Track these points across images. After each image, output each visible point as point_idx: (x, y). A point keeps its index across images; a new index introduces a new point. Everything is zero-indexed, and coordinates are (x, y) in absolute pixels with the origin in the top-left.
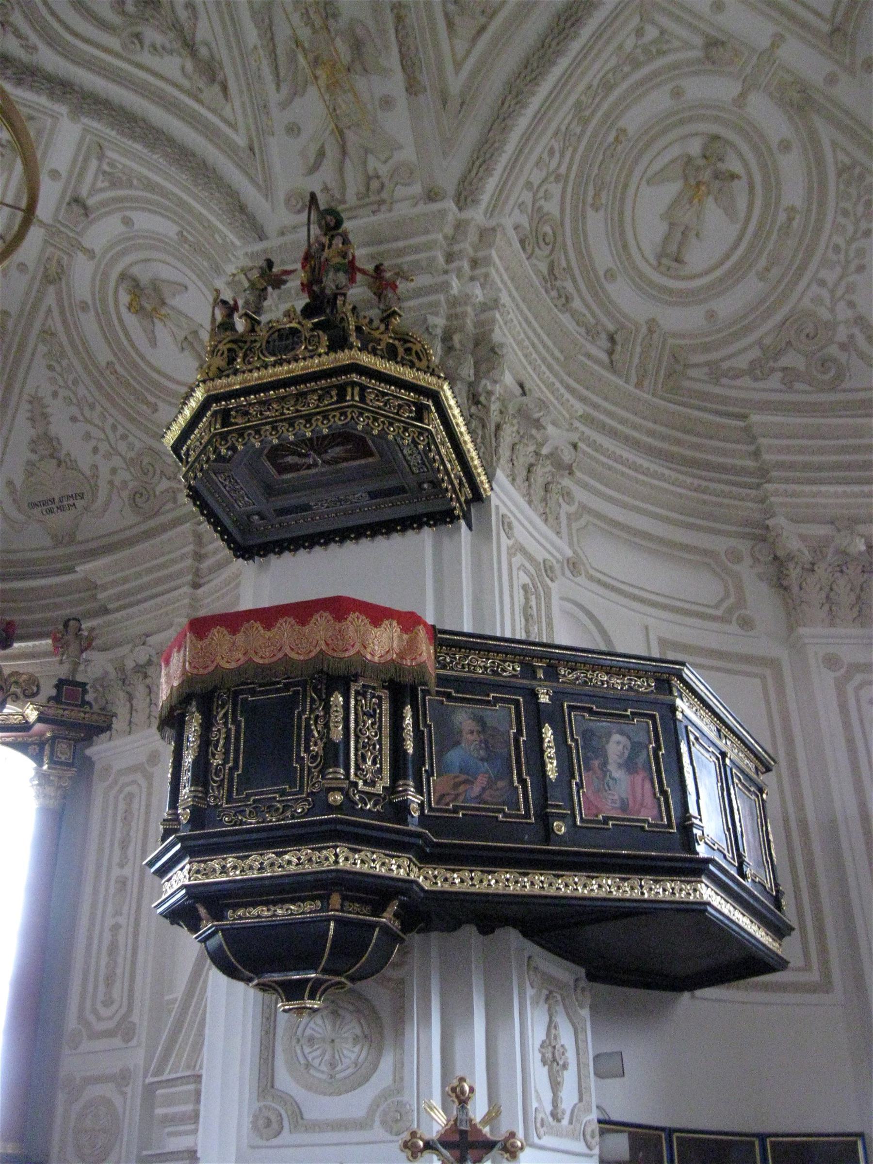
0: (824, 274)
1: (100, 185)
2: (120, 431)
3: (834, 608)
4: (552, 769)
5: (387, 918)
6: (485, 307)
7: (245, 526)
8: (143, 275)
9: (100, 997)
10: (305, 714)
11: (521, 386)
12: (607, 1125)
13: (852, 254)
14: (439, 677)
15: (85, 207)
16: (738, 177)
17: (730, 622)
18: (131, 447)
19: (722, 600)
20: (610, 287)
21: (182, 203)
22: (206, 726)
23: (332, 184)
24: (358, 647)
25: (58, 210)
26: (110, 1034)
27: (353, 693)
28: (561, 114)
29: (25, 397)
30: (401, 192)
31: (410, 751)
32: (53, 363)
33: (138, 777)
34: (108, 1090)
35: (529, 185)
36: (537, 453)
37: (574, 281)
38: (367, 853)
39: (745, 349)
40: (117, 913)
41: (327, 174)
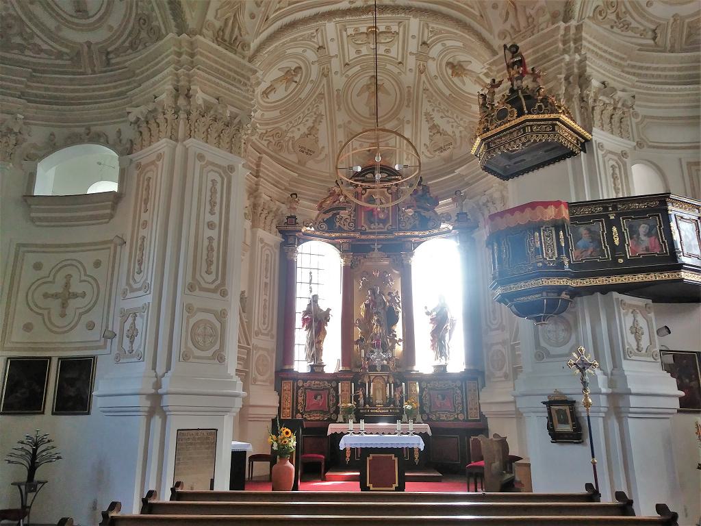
1: (430, 35)
2: (460, 118)
4: (617, 242)
6: (581, 61)
7: (505, 169)
9: (136, 270)
12: (664, 352)
14: (572, 219)
15: (427, 44)
22: (499, 246)
23: (515, 25)
24: (541, 217)
25: (418, 47)
26: (497, 329)
27: (542, 231)
29: (423, 114)
30: (541, 20)
41: (511, 20)
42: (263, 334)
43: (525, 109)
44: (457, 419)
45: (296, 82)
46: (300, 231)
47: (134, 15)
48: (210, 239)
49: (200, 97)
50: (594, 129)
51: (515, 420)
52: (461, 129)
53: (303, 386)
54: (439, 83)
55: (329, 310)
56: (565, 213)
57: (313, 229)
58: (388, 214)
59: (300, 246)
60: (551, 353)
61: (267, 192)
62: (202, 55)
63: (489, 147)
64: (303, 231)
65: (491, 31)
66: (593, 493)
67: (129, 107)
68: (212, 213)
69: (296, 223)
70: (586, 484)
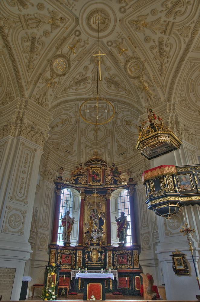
5: (177, 205)
8: (127, 120)
10: (161, 181)
18: (131, 143)
20: (196, 104)
21: (130, 109)
26: (146, 227)
28: (181, 81)
31: (176, 183)
33: (143, 190)
34: (147, 235)
35: (179, 94)
36: (189, 134)
37: (190, 104)
38: (172, 197)
40: (144, 210)
42: (44, 227)
44: (129, 268)
45: (66, 124)
46: (63, 183)
47: (5, 92)
48: (23, 178)
49: (26, 121)
50: (183, 140)
51: (155, 268)
52: (130, 146)
53: (60, 252)
54: (121, 128)
55: (74, 218)
57: (69, 183)
58: (101, 178)
59: (63, 190)
61: (51, 167)
62: (29, 106)
63: (143, 144)
65: (141, 106)
68: (25, 167)
70: (197, 295)
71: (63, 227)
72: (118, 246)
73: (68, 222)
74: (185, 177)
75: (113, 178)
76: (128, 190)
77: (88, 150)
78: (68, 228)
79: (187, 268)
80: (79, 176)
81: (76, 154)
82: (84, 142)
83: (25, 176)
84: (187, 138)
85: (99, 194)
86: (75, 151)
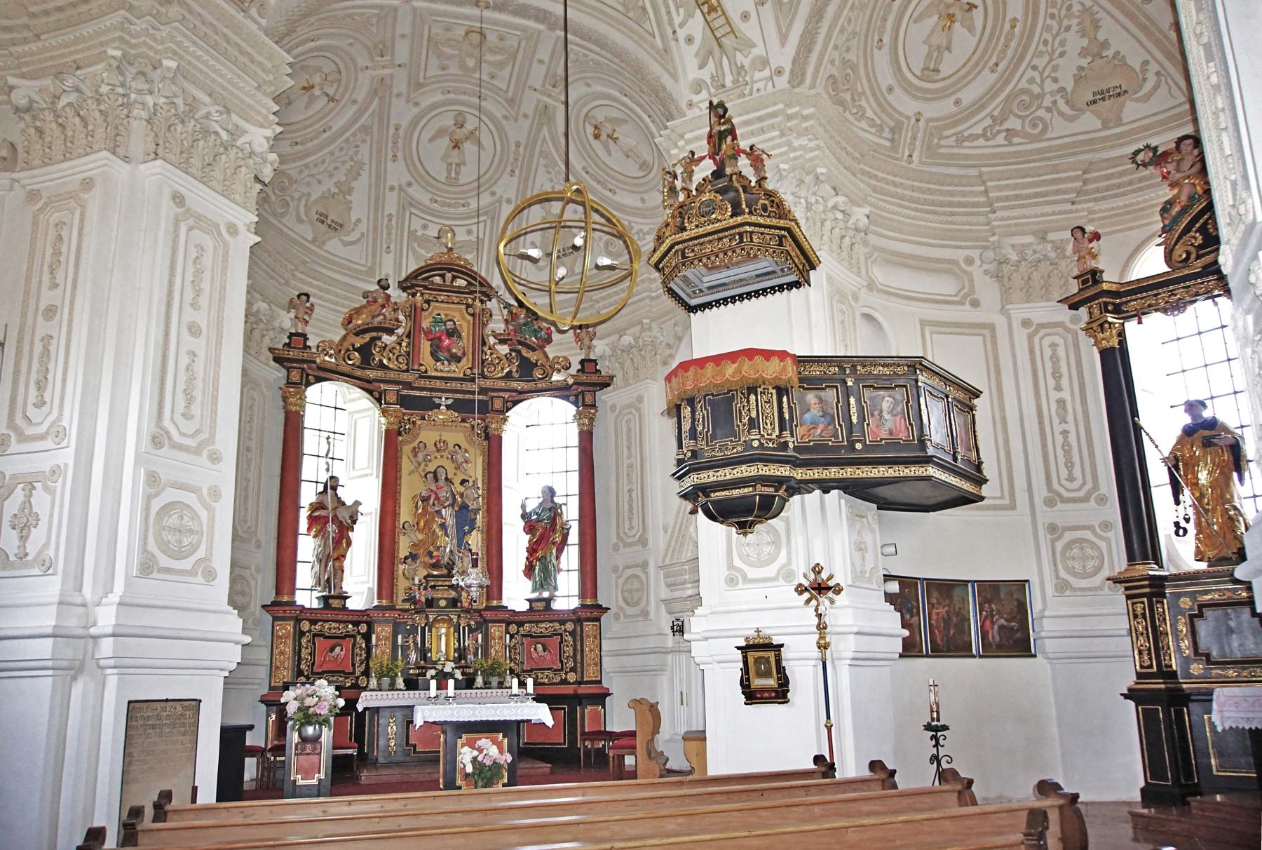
0: (1035, 62)
3: (1031, 290)
4: (854, 419)
5: (781, 492)
10: (737, 405)
11: (834, 189)
12: (888, 578)
13: (1056, 45)
14: (801, 380)
16: (976, 7)
17: (964, 304)
19: (959, 292)
22: (693, 412)
30: (758, 75)
32: (550, 169)
39: (982, 120)
43: (744, 206)
46: (314, 362)
53: (310, 631)
55: (357, 503)
56: (791, 372)
57: (333, 360)
60: (750, 576)
63: (684, 256)
64: (318, 360)
66: (825, 765)
67: (14, 75)
69: (306, 347)
71: (315, 537)
72: (525, 606)
73: (335, 518)
74: (820, 399)
75: (519, 352)
76: (576, 404)
77: (416, 224)
78: (337, 543)
79: (784, 683)
80: (374, 334)
81: (363, 234)
82: (400, 186)
83: (199, 345)
84: (835, 247)
85: (459, 412)
86: (359, 221)
